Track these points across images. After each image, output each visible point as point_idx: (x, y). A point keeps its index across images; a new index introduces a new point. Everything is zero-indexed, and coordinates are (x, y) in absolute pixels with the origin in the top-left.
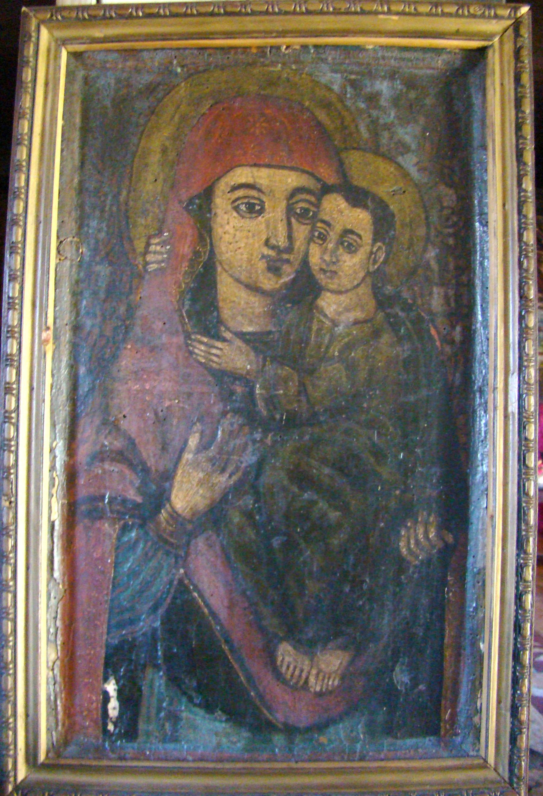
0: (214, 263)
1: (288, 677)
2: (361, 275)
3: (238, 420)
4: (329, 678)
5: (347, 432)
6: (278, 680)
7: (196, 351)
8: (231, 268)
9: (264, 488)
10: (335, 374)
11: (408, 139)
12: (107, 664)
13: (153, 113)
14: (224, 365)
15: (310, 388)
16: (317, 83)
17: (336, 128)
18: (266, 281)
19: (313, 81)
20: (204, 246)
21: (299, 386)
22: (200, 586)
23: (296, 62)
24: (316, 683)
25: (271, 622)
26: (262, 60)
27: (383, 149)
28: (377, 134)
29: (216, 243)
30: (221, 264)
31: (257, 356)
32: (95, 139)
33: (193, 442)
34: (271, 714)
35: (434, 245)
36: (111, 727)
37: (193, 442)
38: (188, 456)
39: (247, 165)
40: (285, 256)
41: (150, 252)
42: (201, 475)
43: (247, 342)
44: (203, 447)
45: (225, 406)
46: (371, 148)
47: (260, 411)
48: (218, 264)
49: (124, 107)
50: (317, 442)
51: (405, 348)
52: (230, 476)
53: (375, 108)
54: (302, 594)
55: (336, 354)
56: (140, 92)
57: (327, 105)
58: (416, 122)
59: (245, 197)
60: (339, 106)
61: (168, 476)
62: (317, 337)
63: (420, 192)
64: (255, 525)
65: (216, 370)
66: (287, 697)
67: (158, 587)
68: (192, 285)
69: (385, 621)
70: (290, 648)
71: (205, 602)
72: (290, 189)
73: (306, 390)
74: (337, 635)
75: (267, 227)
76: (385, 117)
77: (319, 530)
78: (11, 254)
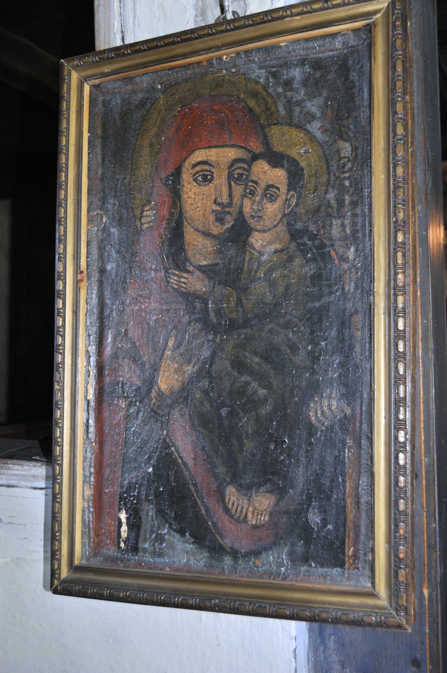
0: (182, 220)
1: (233, 512)
2: (279, 217)
3: (199, 326)
4: (261, 515)
5: (270, 331)
6: (227, 514)
7: (172, 281)
8: (193, 222)
9: (215, 373)
10: (262, 290)
11: (314, 109)
12: (121, 499)
13: (144, 120)
14: (189, 289)
15: (244, 302)
16: (249, 80)
17: (262, 111)
18: (215, 229)
19: (245, 78)
20: (176, 209)
21: (237, 300)
22: (176, 444)
23: (234, 67)
24: (253, 518)
25: (221, 470)
26: (211, 69)
27: (296, 121)
28: (291, 110)
29: (183, 205)
30: (186, 219)
31: (209, 281)
32: (111, 143)
33: (170, 343)
34: (222, 540)
35: (333, 187)
36: (122, 545)
37: (171, 343)
38: (168, 353)
39: (202, 148)
40: (227, 210)
41: (144, 217)
42: (176, 366)
43: (202, 272)
44: (178, 346)
45: (190, 317)
46: (286, 122)
47: (212, 320)
48: (184, 220)
49: (127, 119)
50: (249, 339)
51: (312, 267)
52: (194, 366)
53: (290, 90)
54: (241, 451)
55: (262, 275)
56: (136, 106)
57: (255, 95)
58: (320, 95)
59: (201, 171)
60: (264, 93)
61: (155, 368)
62: (249, 264)
63: (323, 149)
64: (210, 401)
65: (183, 293)
66: (233, 527)
67: (151, 444)
68: (169, 236)
69: (301, 473)
70: (234, 490)
71: (179, 455)
72: (230, 161)
73: (242, 304)
74: (265, 482)
75: (216, 190)
76: (297, 95)
77: (254, 403)
78: (59, 225)
